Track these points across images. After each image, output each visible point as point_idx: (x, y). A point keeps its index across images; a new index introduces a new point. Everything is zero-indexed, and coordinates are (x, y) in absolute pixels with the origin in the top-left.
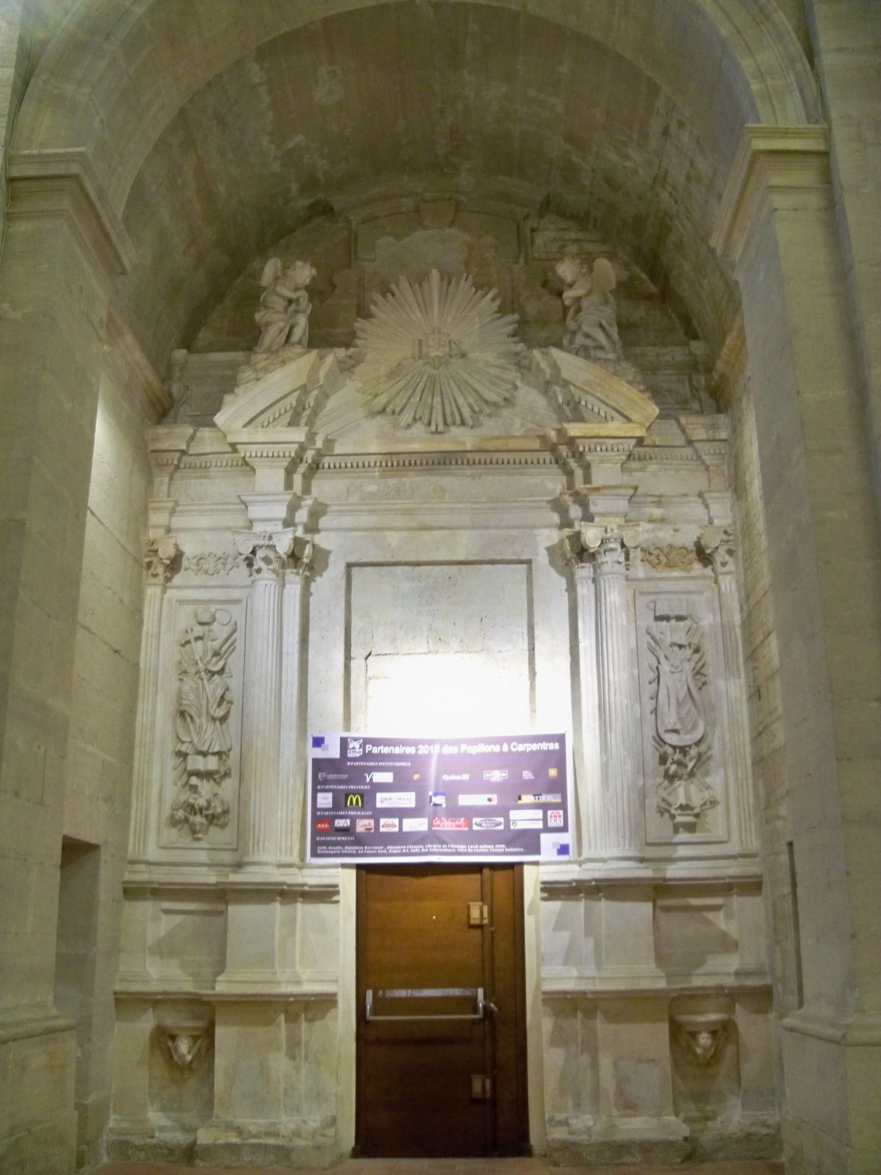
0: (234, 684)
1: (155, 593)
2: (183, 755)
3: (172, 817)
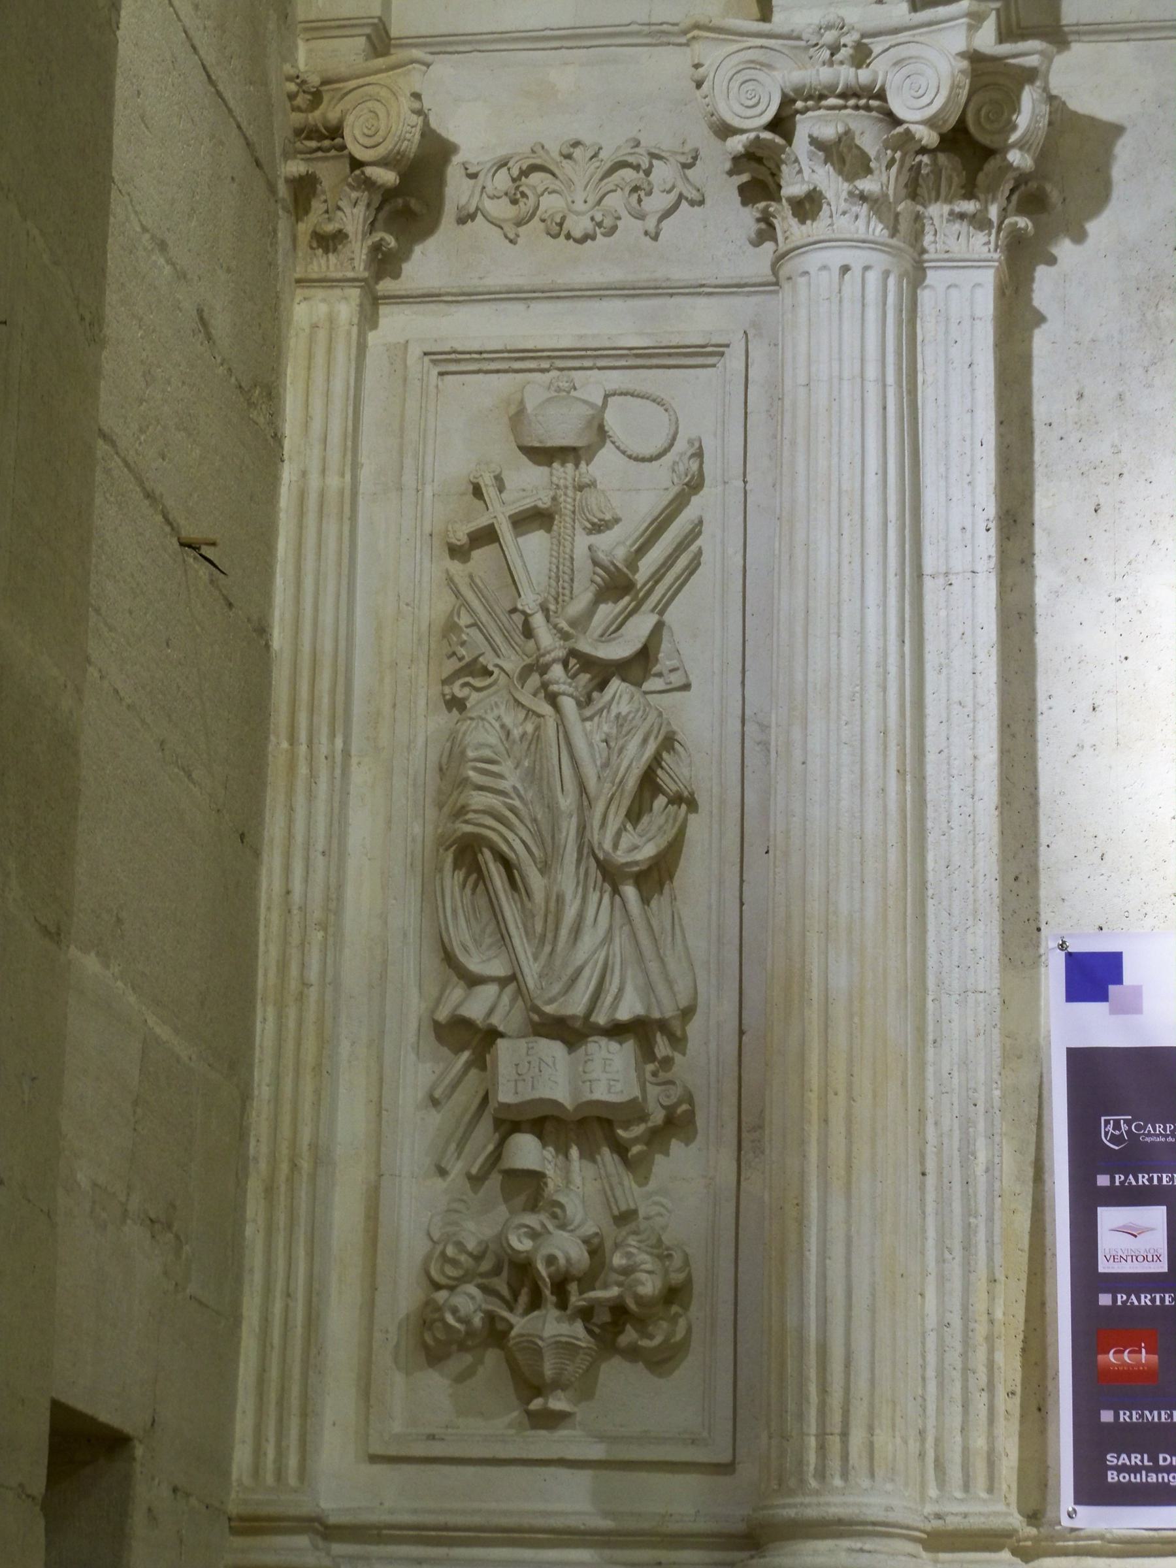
0: (700, 717)
1: (331, 319)
2: (472, 1039)
3: (428, 1318)
